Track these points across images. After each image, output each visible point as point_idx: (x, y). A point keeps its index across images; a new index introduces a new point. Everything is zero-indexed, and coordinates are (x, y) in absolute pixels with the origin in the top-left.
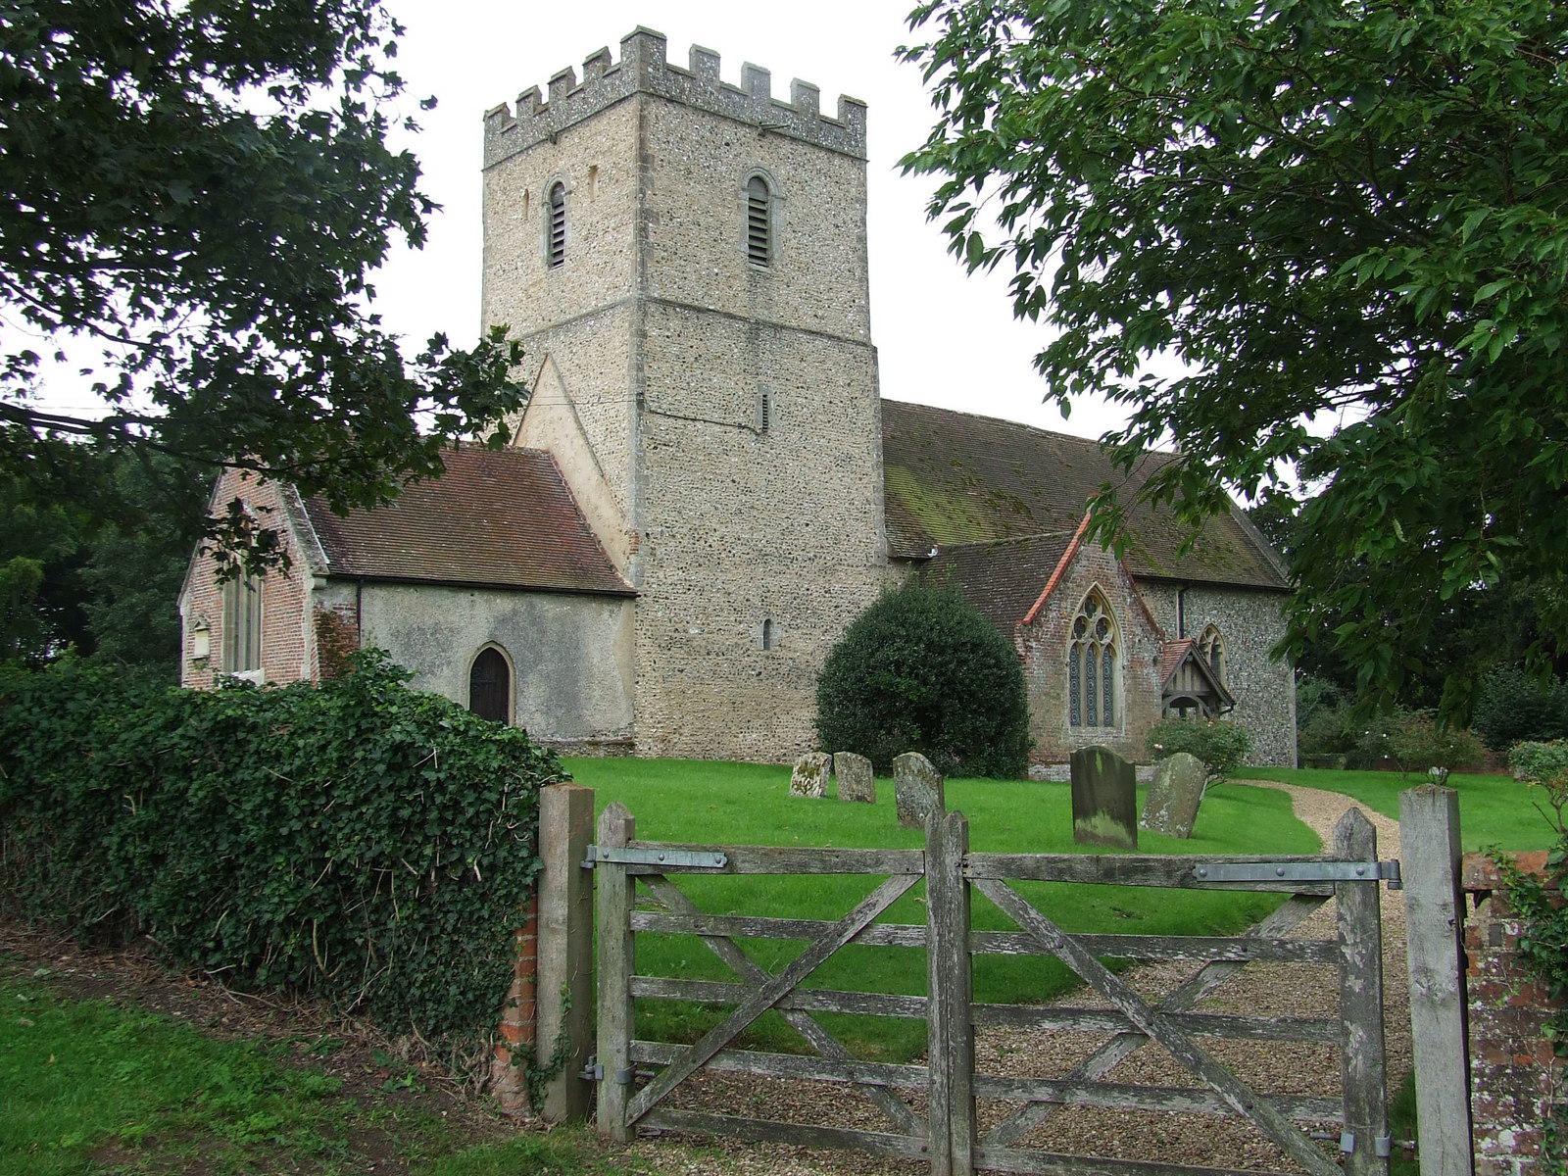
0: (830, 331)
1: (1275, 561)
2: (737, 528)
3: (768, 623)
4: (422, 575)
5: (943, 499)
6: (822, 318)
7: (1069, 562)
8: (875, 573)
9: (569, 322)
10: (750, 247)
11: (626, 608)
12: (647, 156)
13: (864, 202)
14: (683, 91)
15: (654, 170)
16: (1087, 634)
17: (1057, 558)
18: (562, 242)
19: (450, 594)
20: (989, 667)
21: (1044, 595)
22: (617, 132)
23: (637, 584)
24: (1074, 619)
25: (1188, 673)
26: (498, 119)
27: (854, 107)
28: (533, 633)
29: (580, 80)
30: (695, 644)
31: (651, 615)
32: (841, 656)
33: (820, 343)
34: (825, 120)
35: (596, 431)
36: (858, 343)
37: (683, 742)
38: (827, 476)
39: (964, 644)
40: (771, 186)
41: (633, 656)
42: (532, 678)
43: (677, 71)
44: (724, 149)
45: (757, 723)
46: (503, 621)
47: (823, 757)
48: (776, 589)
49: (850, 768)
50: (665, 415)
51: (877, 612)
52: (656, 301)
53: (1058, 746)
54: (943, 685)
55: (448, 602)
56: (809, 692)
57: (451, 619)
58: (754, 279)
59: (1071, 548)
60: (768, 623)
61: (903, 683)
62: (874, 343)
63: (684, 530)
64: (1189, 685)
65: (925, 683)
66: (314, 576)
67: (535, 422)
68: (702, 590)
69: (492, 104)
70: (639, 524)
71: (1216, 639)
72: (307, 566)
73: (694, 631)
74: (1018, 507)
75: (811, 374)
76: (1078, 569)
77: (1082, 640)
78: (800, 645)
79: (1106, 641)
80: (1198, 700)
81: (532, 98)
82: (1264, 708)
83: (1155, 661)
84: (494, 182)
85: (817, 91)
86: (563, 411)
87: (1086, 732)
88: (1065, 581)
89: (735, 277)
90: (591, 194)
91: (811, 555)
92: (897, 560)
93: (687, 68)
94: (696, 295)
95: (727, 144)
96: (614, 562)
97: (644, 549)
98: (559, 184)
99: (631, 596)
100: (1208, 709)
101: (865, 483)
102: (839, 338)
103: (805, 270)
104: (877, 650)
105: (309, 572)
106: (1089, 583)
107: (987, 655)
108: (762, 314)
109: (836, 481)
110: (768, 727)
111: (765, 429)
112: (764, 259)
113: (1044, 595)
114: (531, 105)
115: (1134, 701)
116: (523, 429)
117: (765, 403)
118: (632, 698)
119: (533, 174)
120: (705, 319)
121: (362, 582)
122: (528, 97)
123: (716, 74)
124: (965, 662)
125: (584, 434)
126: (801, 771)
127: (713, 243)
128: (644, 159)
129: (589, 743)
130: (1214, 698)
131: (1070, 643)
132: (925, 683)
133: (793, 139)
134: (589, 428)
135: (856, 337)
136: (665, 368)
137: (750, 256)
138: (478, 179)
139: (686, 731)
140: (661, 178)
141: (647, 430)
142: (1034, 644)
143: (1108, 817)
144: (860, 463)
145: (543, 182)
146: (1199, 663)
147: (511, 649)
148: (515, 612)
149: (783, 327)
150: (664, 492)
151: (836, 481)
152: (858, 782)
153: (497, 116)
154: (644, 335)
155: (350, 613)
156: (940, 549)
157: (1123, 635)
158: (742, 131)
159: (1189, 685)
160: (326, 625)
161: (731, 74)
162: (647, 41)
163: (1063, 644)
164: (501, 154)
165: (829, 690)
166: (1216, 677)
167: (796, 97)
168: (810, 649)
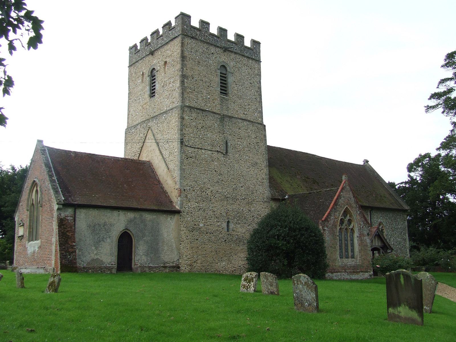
0: (249, 119)
1: (400, 200)
3: (228, 222)
4: (100, 204)
5: (289, 179)
6: (246, 114)
7: (337, 199)
8: (266, 204)
9: (157, 116)
10: (221, 89)
11: (176, 217)
12: (184, 56)
14: (197, 35)
15: (187, 61)
16: (344, 225)
17: (332, 198)
18: (155, 88)
19: (111, 211)
20: (312, 236)
21: (329, 210)
22: (173, 50)
23: (181, 208)
24: (340, 219)
25: (376, 239)
26: (134, 49)
27: (256, 44)
29: (161, 33)
30: (202, 230)
31: (186, 219)
32: (256, 233)
33: (245, 123)
34: (246, 47)
35: (166, 153)
36: (259, 124)
37: (198, 266)
38: (249, 170)
39: (303, 228)
40: (228, 69)
42: (141, 242)
43: (195, 28)
44: (211, 55)
45: (225, 258)
46: (130, 221)
47: (254, 274)
48: (231, 210)
49: (267, 279)
50: (191, 147)
51: (269, 217)
52: (187, 106)
53: (336, 266)
54: (295, 243)
55: (109, 214)
58: (222, 100)
59: (338, 193)
60: (228, 222)
61: (280, 243)
62: (264, 124)
63: (198, 188)
64: (377, 243)
65: (288, 242)
67: (145, 152)
68: (204, 210)
70: (181, 186)
72: (55, 200)
73: (201, 225)
74: (314, 182)
76: (341, 201)
77: (343, 227)
78: (240, 230)
79: (351, 227)
81: (145, 41)
82: (399, 251)
83: (368, 234)
84: (132, 70)
86: (154, 146)
87: (345, 260)
88: (336, 205)
89: (215, 99)
90: (165, 71)
91: (244, 198)
92: (274, 199)
93: (198, 27)
94: (202, 105)
96: (172, 200)
98: (154, 69)
99: (178, 212)
100: (383, 252)
101: (262, 173)
102: (252, 122)
103: (240, 98)
104: (270, 231)
105: (56, 203)
106: (344, 206)
107: (311, 232)
108: (226, 113)
109: (252, 171)
110: (229, 260)
111: (227, 152)
112: (226, 94)
113: (329, 210)
114: (145, 43)
115: (361, 249)
116: (141, 154)
117: (227, 143)
118: (179, 249)
120: (205, 114)
123: (208, 29)
124: (303, 235)
126: (245, 280)
127: (207, 87)
128: (183, 57)
129: (163, 267)
130: (385, 247)
131: (338, 228)
132: (288, 242)
133: (236, 53)
134: (164, 152)
135: (258, 121)
136: (191, 130)
137: (221, 92)
139: (199, 262)
140: (189, 64)
141: (184, 152)
142: (326, 228)
143: (407, 308)
144: (260, 165)
145: (148, 69)
146: (379, 235)
147: (134, 232)
148: (135, 218)
149: (232, 117)
151: (252, 171)
152: (271, 286)
153: (133, 49)
155: (71, 218)
156: (289, 195)
157: (356, 225)
158: (218, 49)
159: (377, 243)
160: (62, 223)
161: (213, 30)
162: (184, 18)
163: (336, 228)
164: (134, 61)
165: (252, 246)
168: (244, 231)
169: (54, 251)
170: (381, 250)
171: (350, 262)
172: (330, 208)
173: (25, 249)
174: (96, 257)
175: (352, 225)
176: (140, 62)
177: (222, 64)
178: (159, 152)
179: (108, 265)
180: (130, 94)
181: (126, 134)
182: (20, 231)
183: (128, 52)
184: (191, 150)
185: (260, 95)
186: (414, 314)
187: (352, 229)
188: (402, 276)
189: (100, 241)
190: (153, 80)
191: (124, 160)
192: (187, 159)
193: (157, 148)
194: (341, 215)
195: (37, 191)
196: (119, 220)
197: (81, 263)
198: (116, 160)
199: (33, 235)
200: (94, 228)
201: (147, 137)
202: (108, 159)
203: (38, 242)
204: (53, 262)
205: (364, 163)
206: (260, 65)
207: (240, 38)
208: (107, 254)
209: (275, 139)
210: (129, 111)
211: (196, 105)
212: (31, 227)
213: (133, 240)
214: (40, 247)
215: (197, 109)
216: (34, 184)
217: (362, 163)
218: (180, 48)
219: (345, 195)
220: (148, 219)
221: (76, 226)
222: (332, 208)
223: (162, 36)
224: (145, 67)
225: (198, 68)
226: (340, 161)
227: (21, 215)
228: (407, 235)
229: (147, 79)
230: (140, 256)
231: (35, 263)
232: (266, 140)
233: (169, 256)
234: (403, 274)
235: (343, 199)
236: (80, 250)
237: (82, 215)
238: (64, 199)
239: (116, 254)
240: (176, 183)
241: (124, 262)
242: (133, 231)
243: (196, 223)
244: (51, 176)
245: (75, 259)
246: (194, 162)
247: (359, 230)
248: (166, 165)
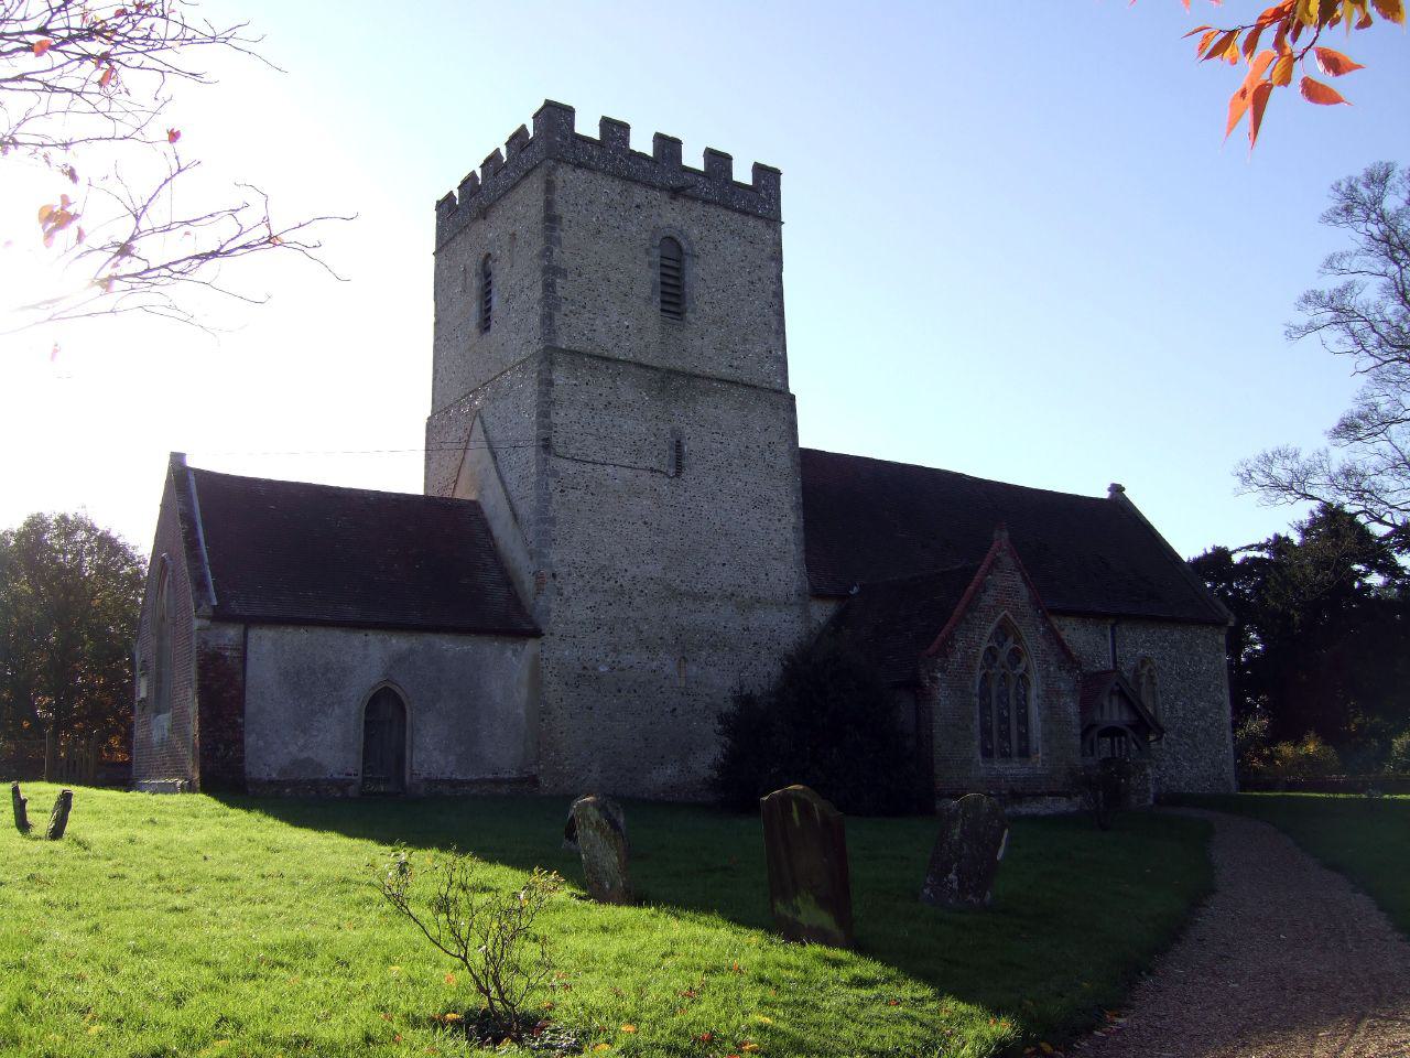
12: (555, 217)
14: (591, 158)
18: (490, 300)
25: (1115, 699)
27: (767, 177)
34: (739, 185)
38: (745, 518)
43: (642, 156)
46: (399, 660)
50: (573, 459)
66: (198, 617)
71: (1150, 670)
80: (1128, 729)
81: (469, 183)
87: (999, 766)
95: (638, 206)
108: (678, 364)
112: (679, 314)
121: (250, 622)
123: (571, 124)
125: (503, 483)
129: (491, 781)
131: (978, 675)
133: (706, 202)
136: (573, 414)
137: (662, 310)
142: (939, 675)
144: (779, 504)
154: (551, 383)
162: (555, 116)
170: (1131, 734)
171: (1013, 769)
174: (304, 755)
175: (1022, 665)
177: (668, 234)
179: (336, 776)
184: (571, 468)
185: (780, 314)
192: (562, 491)
193: (493, 466)
194: (986, 639)
199: (159, 702)
205: (1112, 495)
206: (780, 233)
207: (718, 161)
213: (408, 711)
215: (590, 356)
217: (1105, 494)
221: (249, 674)
223: (505, 165)
224: (469, 259)
225: (596, 248)
228: (1226, 691)
229: (475, 283)
235: (991, 592)
238: (216, 604)
245: (241, 760)
247: (1043, 677)
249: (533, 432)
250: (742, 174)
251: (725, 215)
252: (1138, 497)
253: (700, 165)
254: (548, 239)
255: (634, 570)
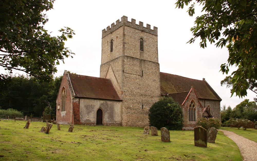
0: (152, 61)
2: (138, 91)
3: (143, 105)
4: (89, 97)
7: (189, 96)
8: (159, 98)
11: (121, 103)
13: (157, 42)
14: (130, 25)
16: (191, 107)
18: (112, 48)
21: (185, 101)
24: (189, 104)
25: (206, 113)
28: (106, 106)
29: (115, 24)
34: (151, 30)
36: (157, 63)
37: (129, 123)
40: (143, 39)
41: (122, 110)
42: (106, 113)
46: (102, 104)
50: (127, 73)
56: (147, 116)
57: (94, 104)
59: (189, 93)
60: (143, 105)
62: (159, 63)
66: (73, 97)
67: (108, 75)
69: (103, 29)
75: (150, 67)
76: (190, 97)
79: (194, 108)
85: (150, 26)
86: (112, 73)
87: (191, 122)
94: (132, 56)
97: (124, 94)
98: (112, 40)
99: (122, 101)
103: (149, 52)
108: (142, 58)
110: (143, 121)
111: (142, 76)
113: (185, 101)
117: (142, 72)
119: (108, 39)
121: (80, 98)
122: (108, 27)
123: (135, 23)
125: (115, 76)
131: (189, 108)
133: (147, 32)
134: (116, 75)
135: (156, 62)
138: (101, 40)
139: (130, 121)
140: (127, 37)
141: (124, 75)
143: (201, 140)
147: (103, 109)
148: (104, 103)
150: (127, 85)
154: (124, 61)
157: (196, 107)
158: (139, 31)
159: (206, 115)
160: (74, 104)
162: (125, 18)
164: (104, 36)
166: (210, 112)
167: (147, 26)
169: (71, 116)
172: (185, 100)
173: (60, 114)
174: (88, 119)
176: (107, 36)
178: (114, 75)
180: (102, 50)
181: (100, 67)
182: (58, 107)
183: (101, 32)
186: (203, 143)
187: (195, 109)
188: (200, 129)
189: (89, 112)
190: (112, 46)
191: (100, 79)
194: (190, 103)
195: (65, 91)
196: (97, 104)
197: (82, 121)
198: (96, 79)
200: (87, 107)
201: (109, 69)
202: (93, 78)
203: (66, 112)
204: (71, 120)
205: (203, 80)
207: (149, 26)
208: (92, 117)
209: (164, 69)
210: (102, 57)
211: (130, 55)
212: (62, 106)
214: (66, 114)
216: (64, 88)
218: (123, 31)
219: (192, 94)
220: (109, 103)
222: (186, 100)
223: (115, 25)
224: (108, 39)
226: (193, 79)
227: (59, 101)
229: (110, 44)
230: (106, 119)
231: (64, 120)
232: (159, 70)
233: (117, 119)
234: (200, 128)
236: (82, 116)
237: (82, 101)
239: (96, 117)
240: (121, 89)
241: (99, 121)
242: (103, 108)
243: (129, 105)
244: (70, 85)
246: (128, 80)
248: (117, 81)
249: (121, 69)
250: (152, 28)
251: (150, 35)
252: (207, 80)
253: (130, 21)
254: (124, 38)
255: (136, 91)
